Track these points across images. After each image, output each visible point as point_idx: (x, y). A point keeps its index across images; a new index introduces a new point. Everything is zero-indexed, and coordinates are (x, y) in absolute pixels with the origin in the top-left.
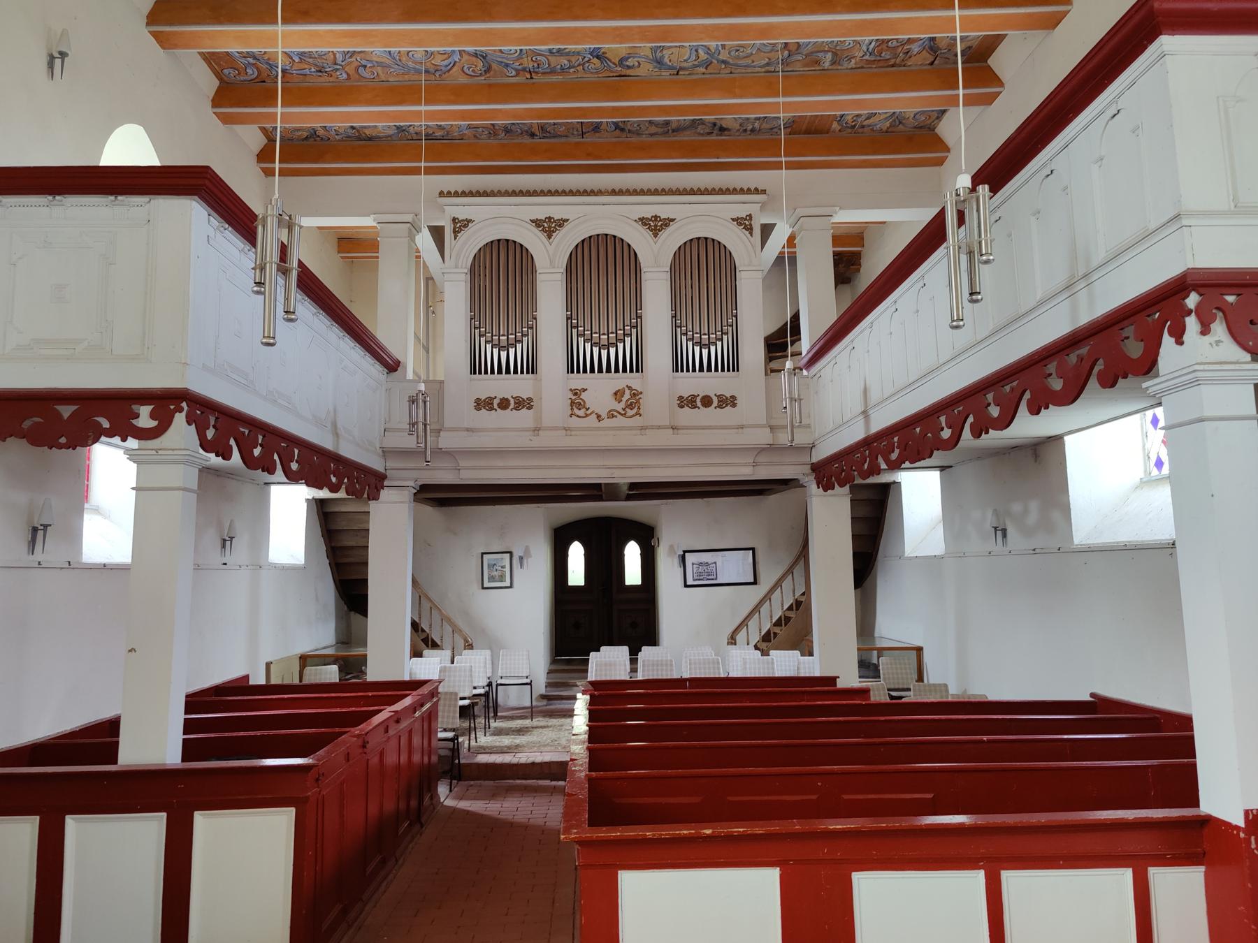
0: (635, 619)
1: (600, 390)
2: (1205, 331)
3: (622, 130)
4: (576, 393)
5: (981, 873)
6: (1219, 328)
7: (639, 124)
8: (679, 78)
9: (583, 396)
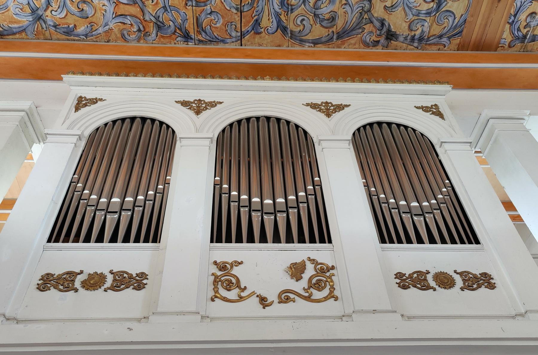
4: (222, 267)
7: (349, 48)
9: (236, 271)
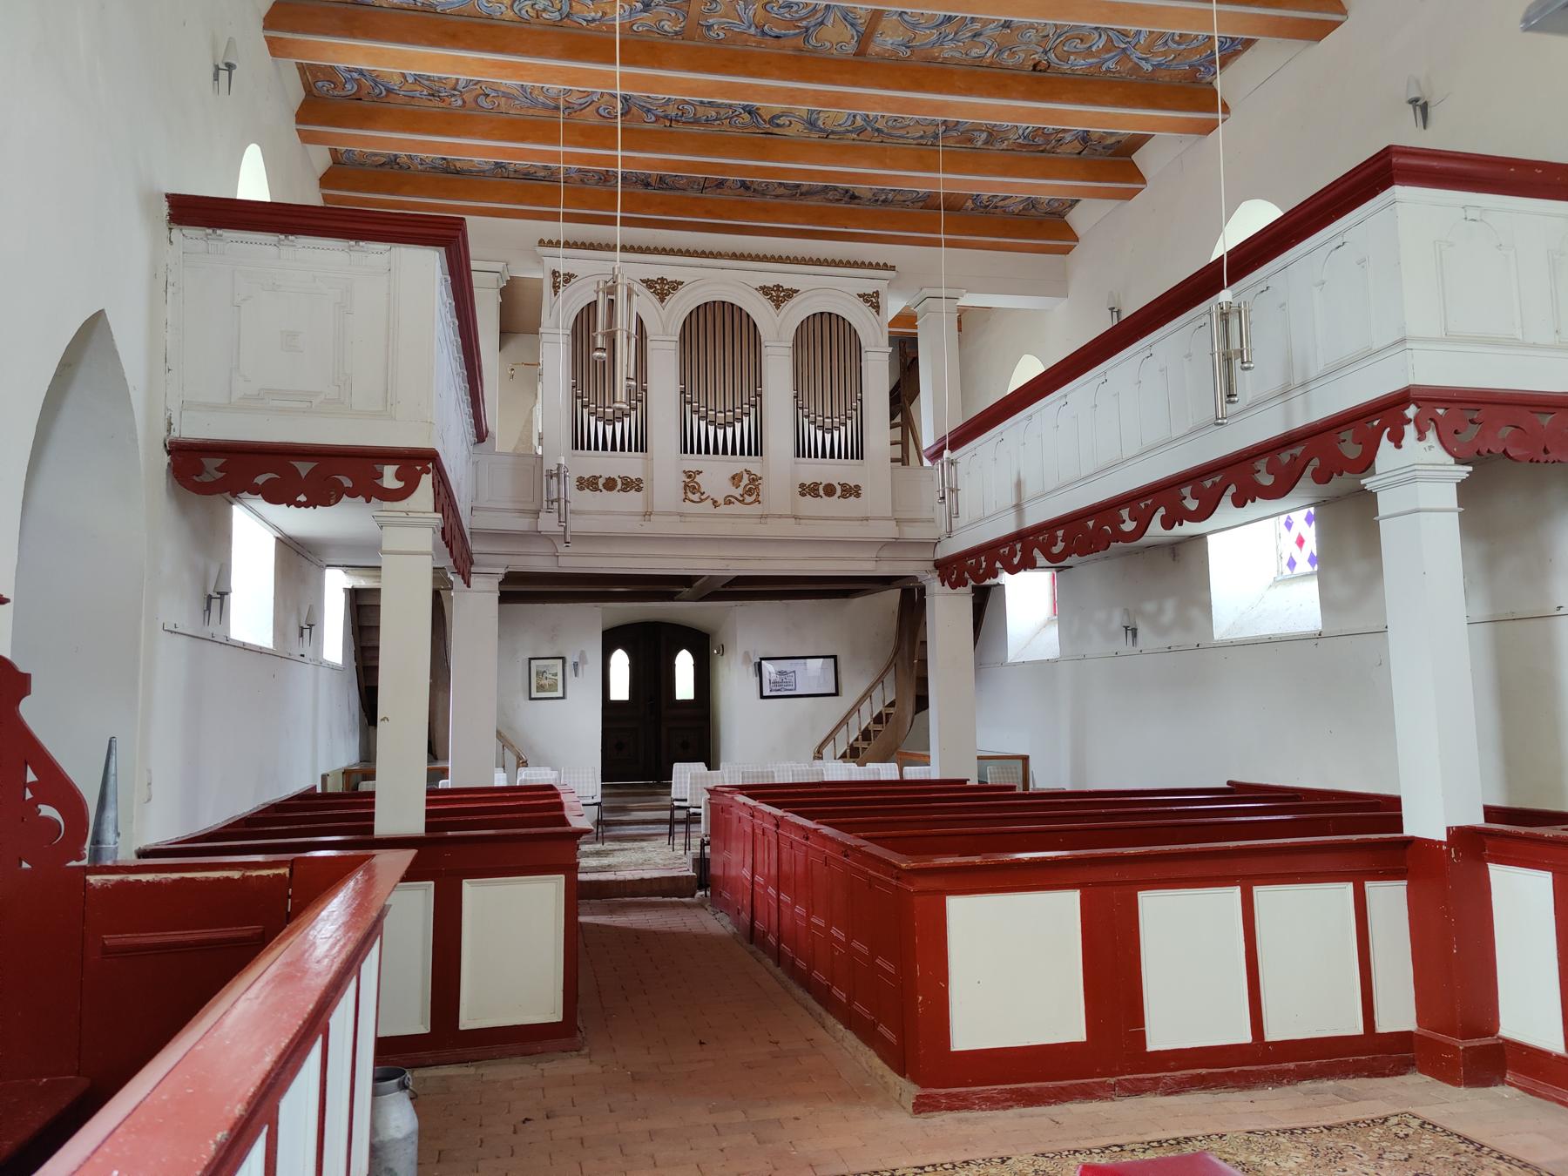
0: (695, 732)
1: (717, 473)
2: (1421, 436)
3: (748, 188)
4: (689, 475)
5: (1238, 889)
6: (1431, 436)
8: (826, 140)
9: (698, 479)
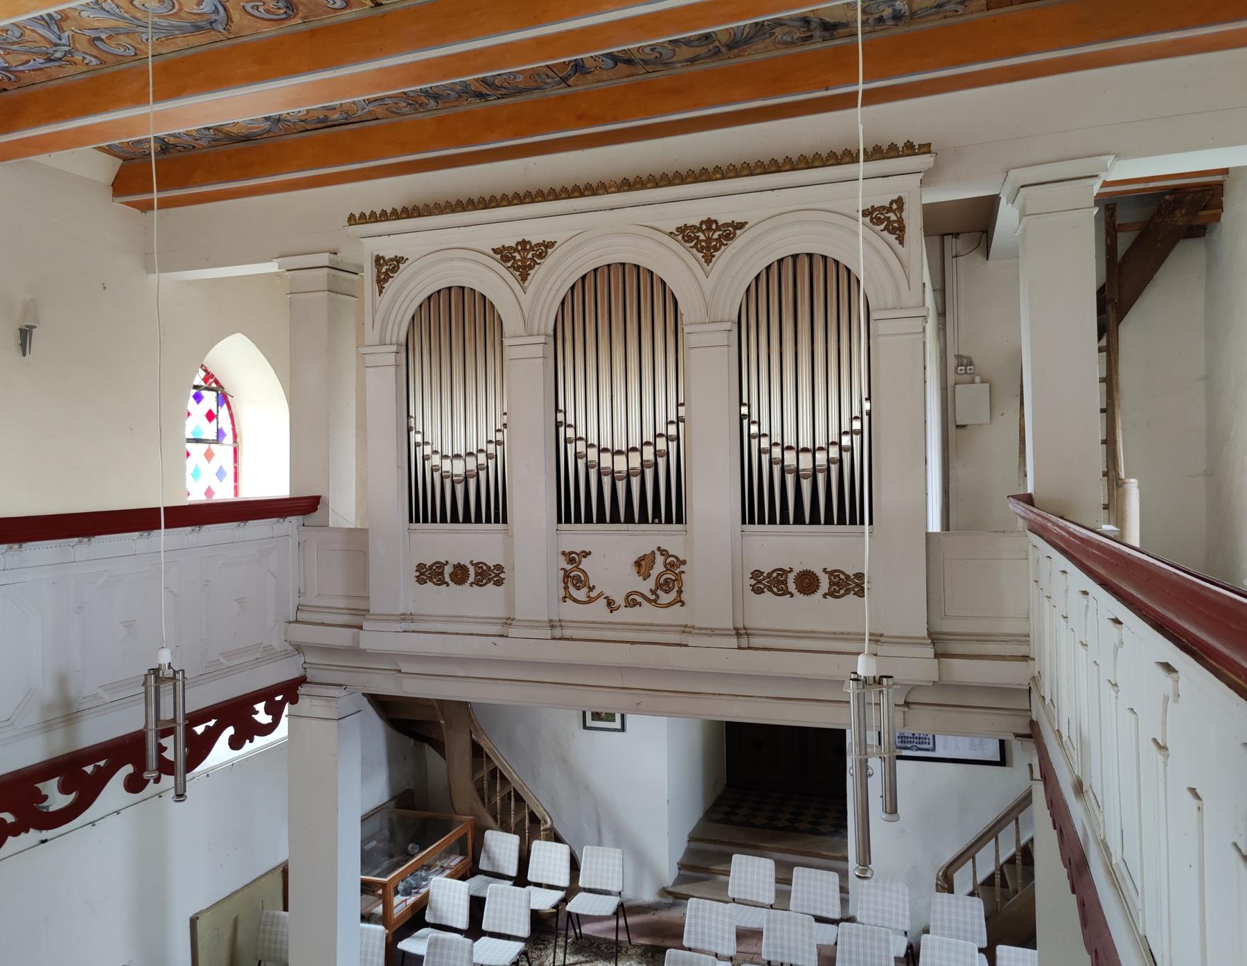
1: (613, 551)
4: (570, 557)
9: (585, 564)
